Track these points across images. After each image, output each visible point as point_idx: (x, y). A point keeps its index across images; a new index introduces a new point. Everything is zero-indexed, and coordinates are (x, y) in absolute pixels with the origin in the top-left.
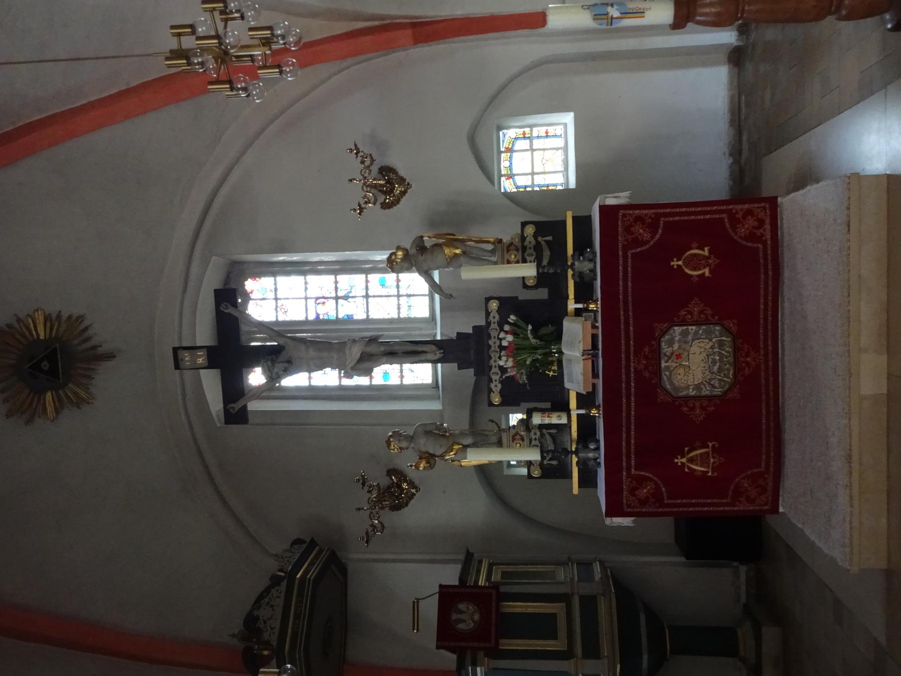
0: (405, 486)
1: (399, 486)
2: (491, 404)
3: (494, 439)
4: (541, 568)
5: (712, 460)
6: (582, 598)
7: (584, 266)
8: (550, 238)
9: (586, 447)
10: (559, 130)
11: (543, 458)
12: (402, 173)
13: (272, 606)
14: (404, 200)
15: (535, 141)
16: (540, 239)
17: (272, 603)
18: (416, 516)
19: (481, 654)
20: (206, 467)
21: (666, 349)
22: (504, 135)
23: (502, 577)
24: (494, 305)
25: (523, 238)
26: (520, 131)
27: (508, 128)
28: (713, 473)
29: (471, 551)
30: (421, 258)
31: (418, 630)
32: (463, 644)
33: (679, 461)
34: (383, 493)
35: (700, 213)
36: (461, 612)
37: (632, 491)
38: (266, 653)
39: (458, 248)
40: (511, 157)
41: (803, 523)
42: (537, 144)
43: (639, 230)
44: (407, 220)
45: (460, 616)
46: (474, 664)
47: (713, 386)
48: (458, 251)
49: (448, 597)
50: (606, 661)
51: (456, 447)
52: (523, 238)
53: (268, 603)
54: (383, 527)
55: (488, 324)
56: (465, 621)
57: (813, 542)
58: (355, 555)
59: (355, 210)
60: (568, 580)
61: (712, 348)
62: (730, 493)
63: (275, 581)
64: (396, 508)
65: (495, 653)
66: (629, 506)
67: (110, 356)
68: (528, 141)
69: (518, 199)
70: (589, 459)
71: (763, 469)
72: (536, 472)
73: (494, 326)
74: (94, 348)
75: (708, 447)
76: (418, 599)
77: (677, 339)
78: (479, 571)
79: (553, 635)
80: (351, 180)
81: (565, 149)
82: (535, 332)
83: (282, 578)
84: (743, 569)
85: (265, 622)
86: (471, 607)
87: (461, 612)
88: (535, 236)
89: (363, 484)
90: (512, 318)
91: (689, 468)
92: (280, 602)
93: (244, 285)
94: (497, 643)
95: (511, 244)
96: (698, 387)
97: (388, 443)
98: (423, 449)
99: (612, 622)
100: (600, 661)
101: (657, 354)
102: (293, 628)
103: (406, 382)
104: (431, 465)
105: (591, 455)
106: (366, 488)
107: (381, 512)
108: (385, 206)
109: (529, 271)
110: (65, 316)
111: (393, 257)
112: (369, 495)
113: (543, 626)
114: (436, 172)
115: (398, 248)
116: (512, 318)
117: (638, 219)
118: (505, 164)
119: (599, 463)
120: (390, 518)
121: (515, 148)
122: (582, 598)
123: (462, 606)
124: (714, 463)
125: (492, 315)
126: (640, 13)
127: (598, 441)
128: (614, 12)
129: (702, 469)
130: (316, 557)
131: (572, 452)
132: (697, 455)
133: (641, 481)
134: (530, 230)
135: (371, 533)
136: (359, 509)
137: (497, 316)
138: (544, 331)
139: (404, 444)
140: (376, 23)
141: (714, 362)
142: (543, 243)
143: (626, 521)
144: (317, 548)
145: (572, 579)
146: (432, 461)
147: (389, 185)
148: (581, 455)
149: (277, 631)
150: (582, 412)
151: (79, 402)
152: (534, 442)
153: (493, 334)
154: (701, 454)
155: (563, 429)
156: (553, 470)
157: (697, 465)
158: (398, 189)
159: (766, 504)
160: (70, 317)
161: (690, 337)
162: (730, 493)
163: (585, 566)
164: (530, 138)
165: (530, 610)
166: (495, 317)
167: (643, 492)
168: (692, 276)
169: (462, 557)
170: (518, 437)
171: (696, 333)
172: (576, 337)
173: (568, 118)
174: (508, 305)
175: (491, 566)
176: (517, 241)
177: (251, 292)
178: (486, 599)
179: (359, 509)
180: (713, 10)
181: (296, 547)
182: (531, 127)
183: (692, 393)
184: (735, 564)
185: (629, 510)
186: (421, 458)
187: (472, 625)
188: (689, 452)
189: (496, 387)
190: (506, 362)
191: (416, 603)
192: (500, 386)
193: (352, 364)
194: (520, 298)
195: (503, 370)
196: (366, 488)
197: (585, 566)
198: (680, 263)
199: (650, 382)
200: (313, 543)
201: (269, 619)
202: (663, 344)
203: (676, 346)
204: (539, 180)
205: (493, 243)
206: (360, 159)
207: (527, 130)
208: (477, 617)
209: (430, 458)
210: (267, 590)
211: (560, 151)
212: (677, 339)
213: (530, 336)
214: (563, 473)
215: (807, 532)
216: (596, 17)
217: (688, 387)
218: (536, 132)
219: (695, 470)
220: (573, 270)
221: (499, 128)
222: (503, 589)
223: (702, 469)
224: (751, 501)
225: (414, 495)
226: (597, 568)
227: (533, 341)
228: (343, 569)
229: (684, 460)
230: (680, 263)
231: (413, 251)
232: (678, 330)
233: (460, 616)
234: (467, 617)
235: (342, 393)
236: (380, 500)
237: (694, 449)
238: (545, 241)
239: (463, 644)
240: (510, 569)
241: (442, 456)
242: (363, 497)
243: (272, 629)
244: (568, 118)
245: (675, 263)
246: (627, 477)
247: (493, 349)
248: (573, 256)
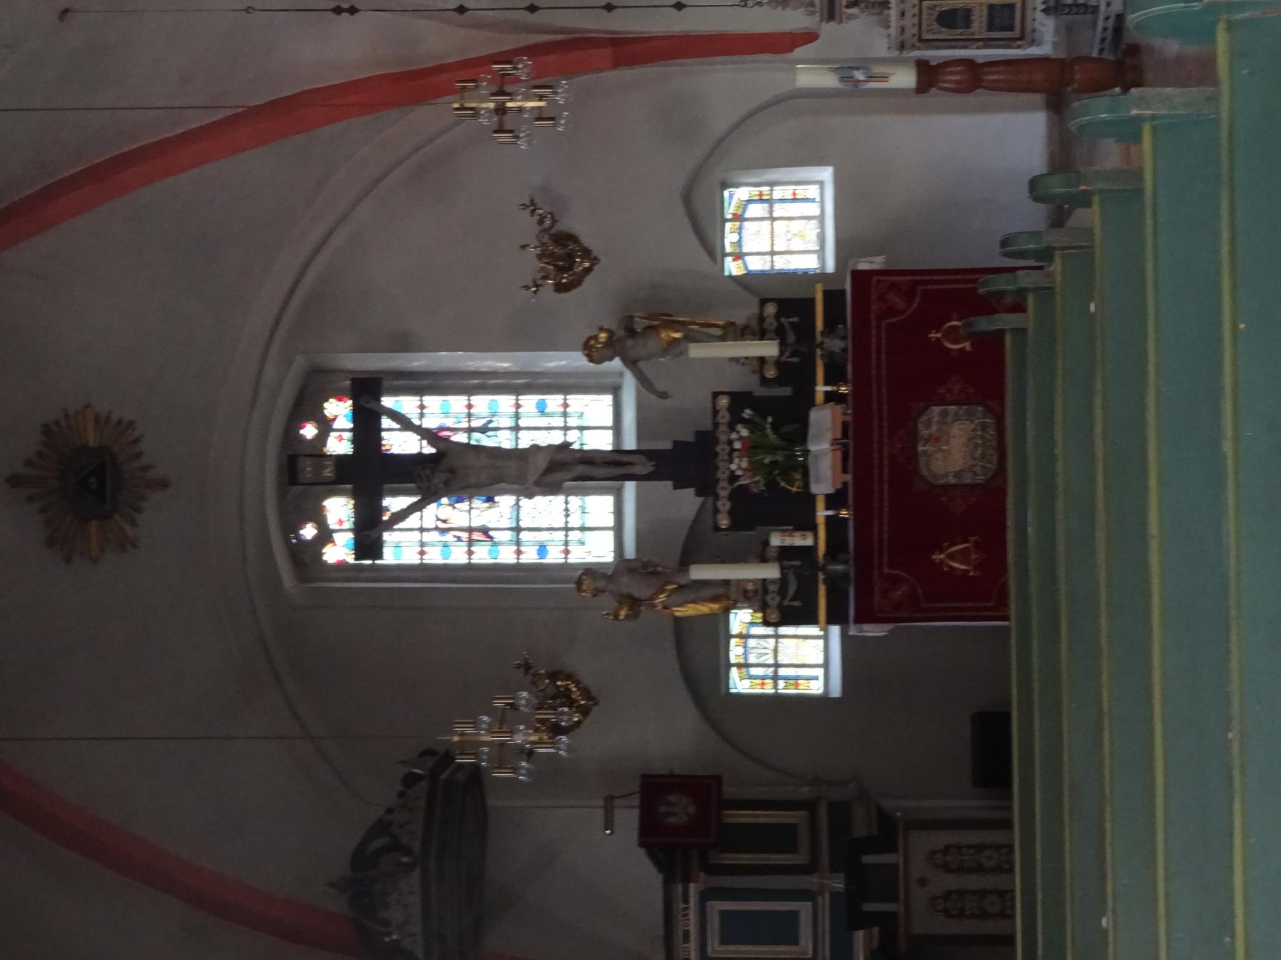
2: (717, 528)
6: (833, 806)
7: (836, 345)
8: (795, 319)
10: (813, 191)
11: (782, 353)
12: (587, 241)
14: (588, 281)
15: (777, 207)
16: (783, 320)
21: (924, 432)
22: (731, 196)
24: (724, 402)
25: (762, 319)
26: (754, 191)
27: (737, 185)
30: (630, 343)
35: (958, 282)
39: (677, 331)
40: (740, 228)
42: (779, 210)
43: (897, 301)
44: (591, 304)
46: (686, 880)
47: (975, 474)
48: (677, 335)
52: (762, 319)
55: (716, 425)
59: (527, 288)
61: (974, 430)
67: (164, 484)
68: (766, 205)
69: (749, 282)
73: (723, 428)
74: (146, 468)
75: (968, 542)
77: (936, 419)
79: (793, 850)
80: (523, 247)
81: (821, 219)
82: (775, 427)
88: (778, 316)
90: (747, 413)
93: (323, 408)
95: (746, 327)
96: (958, 474)
98: (626, 591)
101: (913, 438)
103: (573, 559)
104: (634, 615)
108: (560, 288)
109: (769, 349)
110: (115, 419)
111: (592, 342)
113: (781, 838)
114: (634, 241)
115: (601, 329)
116: (747, 413)
117: (893, 286)
118: (730, 238)
121: (746, 216)
122: (833, 806)
123: (672, 798)
125: (721, 414)
126: (884, 78)
128: (859, 75)
129: (963, 567)
134: (771, 309)
137: (728, 416)
138: (786, 429)
140: (561, 37)
141: (976, 446)
142: (787, 326)
147: (565, 258)
150: (830, 513)
151: (126, 544)
153: (723, 438)
155: (812, 550)
158: (581, 264)
160: (120, 422)
161: (950, 419)
164: (770, 202)
165: (762, 820)
166: (724, 417)
167: (898, 594)
168: (951, 350)
171: (956, 413)
172: (824, 423)
173: (826, 174)
174: (739, 400)
176: (754, 323)
177: (334, 420)
180: (958, 77)
182: (772, 184)
183: (952, 480)
189: (724, 505)
190: (739, 465)
192: (728, 505)
193: (534, 478)
194: (756, 394)
195: (733, 478)
198: (939, 335)
199: (906, 466)
202: (920, 426)
203: (934, 428)
204: (782, 264)
205: (722, 327)
206: (537, 218)
207: (765, 189)
211: (814, 222)
212: (936, 419)
213: (769, 431)
216: (842, 79)
217: (946, 475)
218: (778, 192)
219: (955, 569)
220: (822, 349)
221: (725, 185)
223: (963, 567)
227: (772, 437)
229: (942, 556)
230: (939, 335)
231: (621, 333)
232: (936, 410)
235: (471, 574)
238: (791, 323)
244: (826, 174)
245: (934, 335)
247: (720, 457)
248: (822, 333)
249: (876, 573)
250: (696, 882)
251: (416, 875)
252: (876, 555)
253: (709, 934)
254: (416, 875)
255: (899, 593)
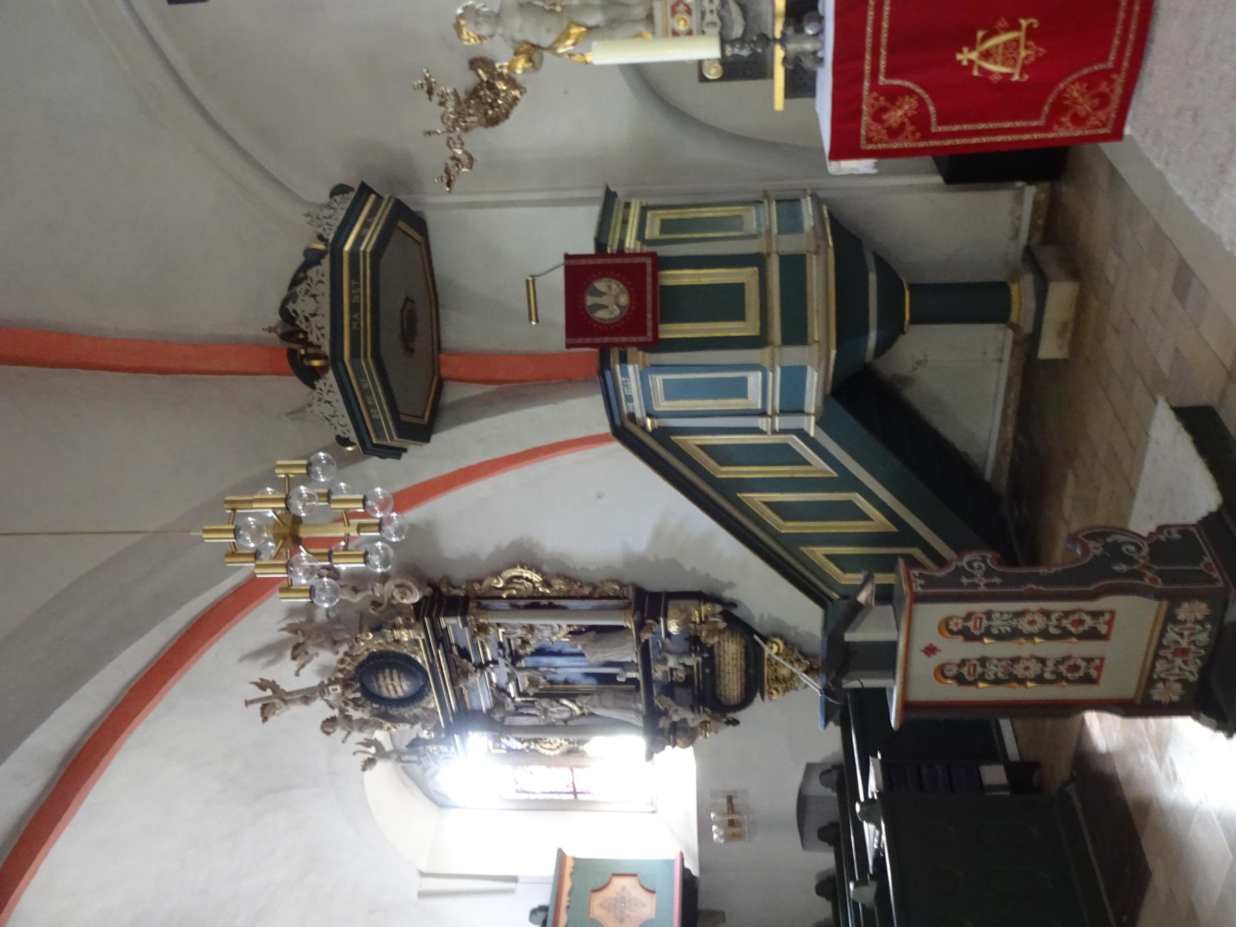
0: (501, 86)
1: (491, 87)
3: (640, 12)
4: (720, 212)
5: (1023, 53)
6: (785, 260)
9: (800, 30)
13: (314, 296)
17: (313, 291)
18: (529, 131)
19: (631, 351)
20: (171, 68)
23: (662, 231)
28: (1021, 75)
29: (612, 189)
31: (537, 321)
32: (606, 340)
33: (965, 56)
34: (467, 101)
36: (601, 294)
37: (877, 116)
38: (316, 363)
41: (1167, 164)
45: (598, 300)
46: (624, 360)
49: (579, 274)
50: (815, 347)
51: (575, 31)
53: (307, 291)
54: (471, 158)
56: (606, 307)
57: (1180, 199)
58: (435, 203)
60: (763, 230)
62: (1046, 109)
63: (312, 259)
64: (493, 122)
65: (658, 345)
66: (869, 140)
70: (804, 53)
71: (1110, 65)
72: (713, 71)
75: (1017, 27)
76: (532, 276)
78: (625, 222)
79: (739, 315)
83: (321, 254)
84: (1030, 192)
85: (307, 320)
86: (614, 286)
87: (601, 294)
89: (430, 92)
91: (981, 69)
92: (325, 288)
94: (656, 331)
97: (458, 28)
98: (519, 37)
99: (827, 274)
100: (807, 349)
102: (351, 325)
105: (808, 46)
106: (436, 99)
107: (465, 137)
112: (442, 109)
113: (726, 302)
119: (821, 61)
120: (481, 140)
122: (785, 260)
123: (601, 285)
124: (1026, 58)
127: (821, 19)
130: (372, 214)
131: (775, 40)
132: (997, 46)
133: (893, 96)
135: (453, 170)
136: (429, 133)
139: (485, 30)
143: (864, 166)
144: (373, 197)
145: (769, 231)
146: (536, 57)
148: (793, 47)
149: (327, 331)
152: (709, 18)
154: (1006, 44)
156: (743, 67)
157: (995, 63)
159: (1104, 125)
162: (1046, 109)
163: (789, 205)
167: (895, 116)
169: (600, 193)
170: (681, 8)
175: (644, 210)
178: (636, 272)
179: (429, 133)
181: (338, 198)
184: (1019, 184)
185: (870, 147)
186: (517, 53)
187: (617, 311)
188: (985, 39)
191: (531, 284)
196: (436, 99)
197: (789, 205)
200: (365, 190)
201: (314, 315)
208: (624, 300)
209: (532, 52)
210: (304, 268)
214: (756, 69)
215: (1172, 178)
222: (663, 251)
224: (1078, 121)
225: (516, 99)
226: (807, 207)
228: (419, 224)
229: (974, 56)
233: (598, 300)
234: (609, 300)
236: (460, 114)
237: (992, 33)
239: (606, 340)
240: (674, 215)
241: (552, 48)
242: (431, 114)
243: (320, 329)
246: (871, 90)
249: (866, 84)
250: (633, 363)
251: (330, 375)
252: (868, 57)
253: (679, 211)
254: (330, 375)
255: (900, 113)
